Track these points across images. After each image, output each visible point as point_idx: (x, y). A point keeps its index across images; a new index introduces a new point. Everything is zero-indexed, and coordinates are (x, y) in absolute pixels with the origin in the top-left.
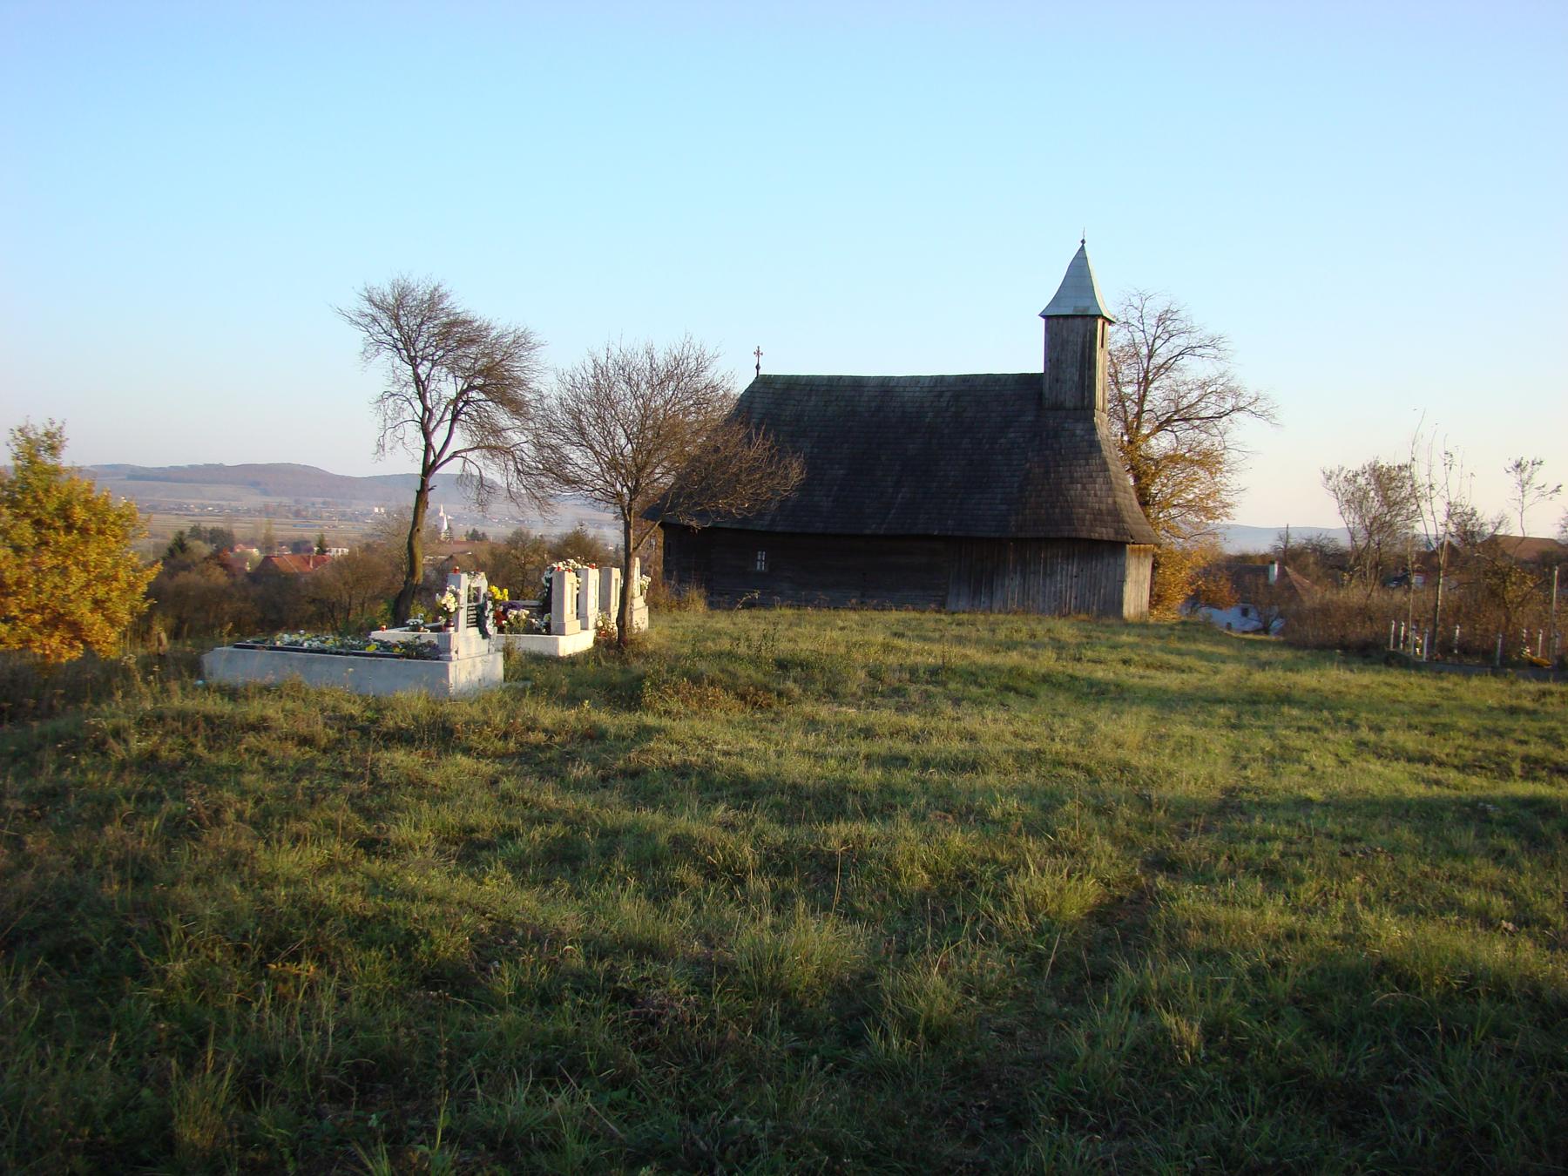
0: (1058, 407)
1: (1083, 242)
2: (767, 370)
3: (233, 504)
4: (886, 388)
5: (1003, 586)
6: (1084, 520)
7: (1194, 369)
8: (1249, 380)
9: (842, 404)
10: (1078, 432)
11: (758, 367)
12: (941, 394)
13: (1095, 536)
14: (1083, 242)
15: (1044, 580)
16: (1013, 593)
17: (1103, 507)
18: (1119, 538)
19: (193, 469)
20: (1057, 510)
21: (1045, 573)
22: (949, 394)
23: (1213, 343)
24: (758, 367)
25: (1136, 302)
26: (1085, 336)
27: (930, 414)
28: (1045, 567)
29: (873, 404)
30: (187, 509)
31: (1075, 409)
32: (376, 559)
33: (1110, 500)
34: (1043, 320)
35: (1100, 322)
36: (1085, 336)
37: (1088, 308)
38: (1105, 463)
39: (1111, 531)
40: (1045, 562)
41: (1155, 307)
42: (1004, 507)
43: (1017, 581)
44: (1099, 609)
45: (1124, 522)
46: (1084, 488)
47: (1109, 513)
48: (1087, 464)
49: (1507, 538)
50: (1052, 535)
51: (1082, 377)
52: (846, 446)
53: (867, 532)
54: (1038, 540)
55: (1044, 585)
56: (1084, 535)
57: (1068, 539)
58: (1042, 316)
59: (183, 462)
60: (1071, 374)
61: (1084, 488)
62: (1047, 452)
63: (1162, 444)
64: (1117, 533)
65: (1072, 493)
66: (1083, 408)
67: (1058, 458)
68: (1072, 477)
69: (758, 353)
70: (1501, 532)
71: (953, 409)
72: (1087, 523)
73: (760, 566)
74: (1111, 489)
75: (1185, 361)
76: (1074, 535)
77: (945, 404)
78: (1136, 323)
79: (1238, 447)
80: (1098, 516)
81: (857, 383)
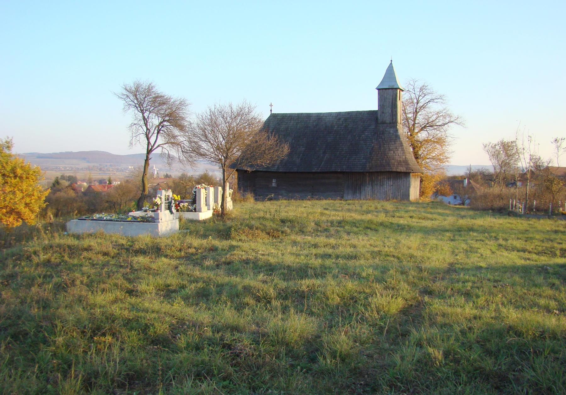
0: (384, 123)
1: (391, 61)
2: (272, 112)
3: (77, 166)
4: (319, 117)
5: (365, 190)
6: (394, 164)
7: (434, 107)
8: (455, 111)
9: (303, 123)
10: (391, 132)
11: (271, 111)
12: (340, 119)
13: (399, 170)
14: (391, 61)
15: (380, 187)
16: (369, 192)
17: (401, 159)
18: (408, 171)
19: (61, 153)
20: (384, 161)
21: (380, 185)
22: (343, 119)
23: (441, 97)
24: (271, 111)
25: (412, 83)
26: (393, 96)
27: (336, 127)
28: (380, 182)
29: (314, 123)
30: (59, 169)
31: (390, 123)
32: (130, 185)
33: (404, 157)
34: (377, 91)
35: (398, 90)
36: (393, 96)
37: (394, 86)
38: (402, 143)
39: (405, 168)
40: (380, 180)
41: (419, 84)
42: (364, 160)
43: (370, 187)
44: (400, 198)
45: (409, 165)
46: (394, 153)
47: (404, 162)
48: (395, 144)
49: (552, 167)
50: (382, 170)
51: (392, 111)
52: (305, 139)
53: (314, 171)
54: (377, 172)
55: (380, 189)
56: (394, 170)
57: (389, 172)
58: (377, 89)
59: (58, 151)
60: (388, 110)
61: (394, 153)
62: (380, 140)
63: (422, 135)
64: (407, 169)
65: (390, 154)
66: (393, 123)
67: (384, 141)
68: (389, 149)
69: (271, 105)
70: (550, 165)
71: (344, 124)
72: (395, 165)
73: (274, 185)
74: (404, 153)
75: (431, 104)
76: (390, 170)
77: (341, 123)
78: (412, 91)
79: (452, 136)
80: (399, 163)
81: (308, 116)
